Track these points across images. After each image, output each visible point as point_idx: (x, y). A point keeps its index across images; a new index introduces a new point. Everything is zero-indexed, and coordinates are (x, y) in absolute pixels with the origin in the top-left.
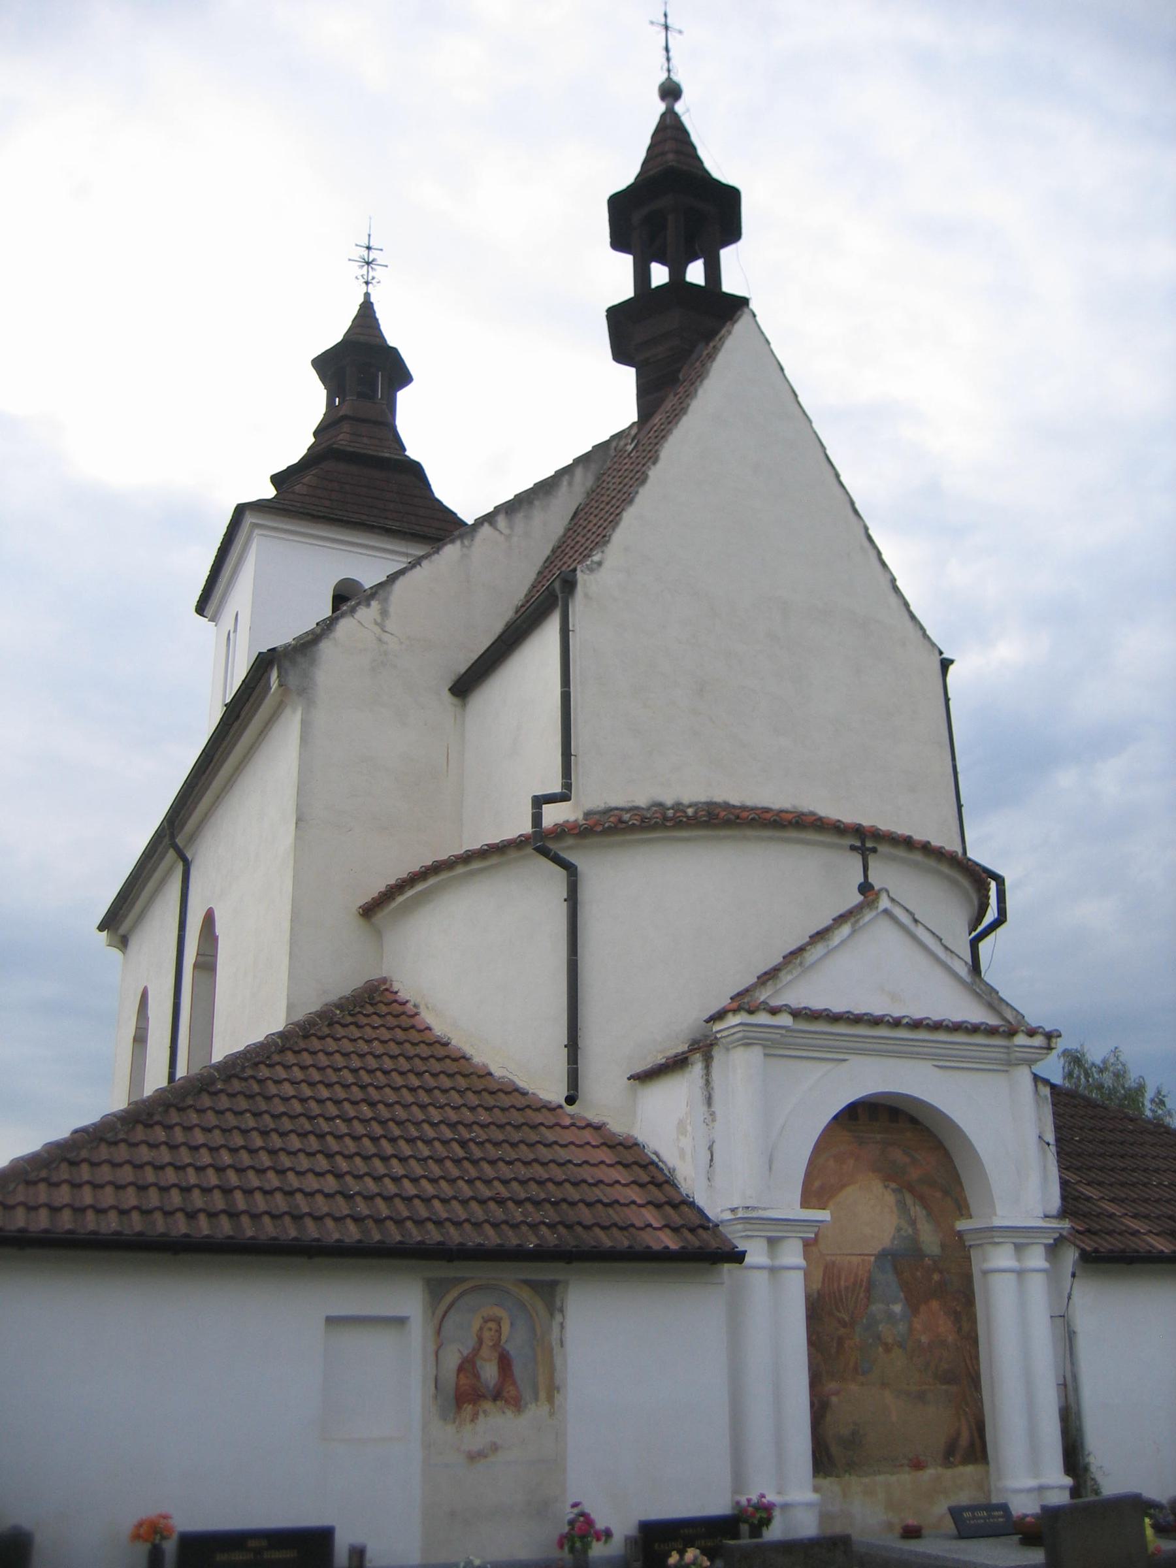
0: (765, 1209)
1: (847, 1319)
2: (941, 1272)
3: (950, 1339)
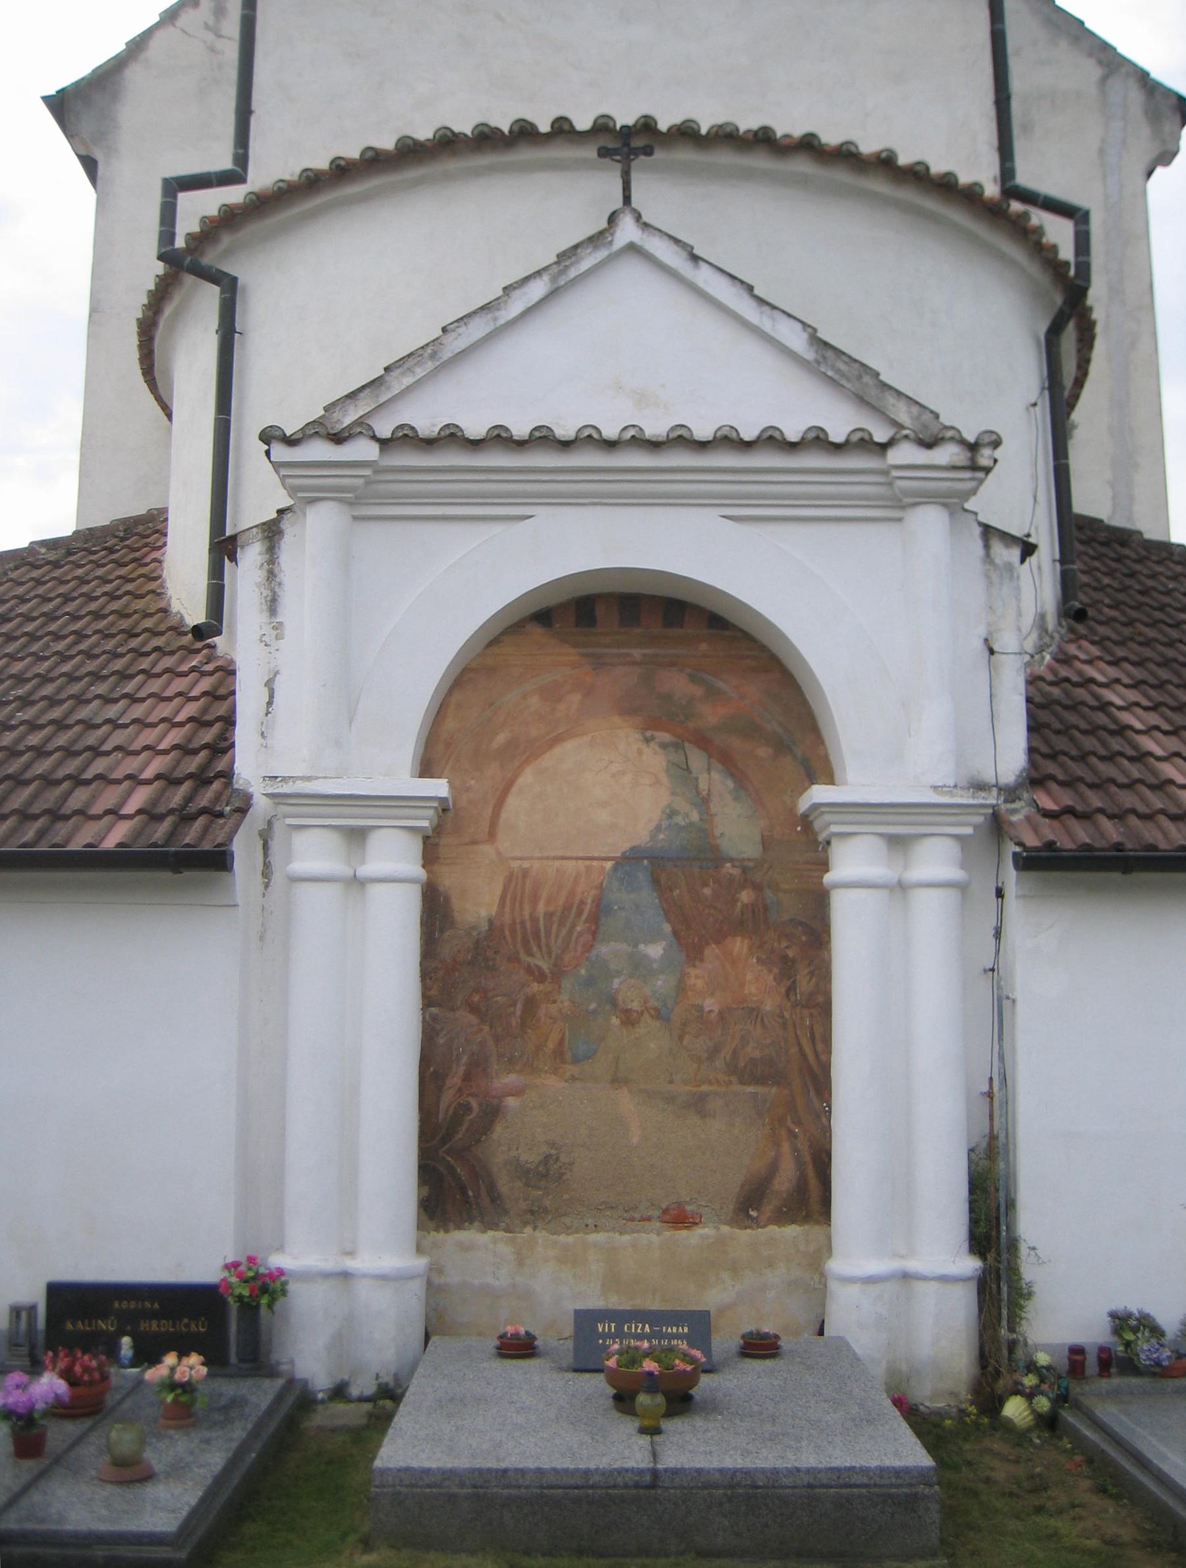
0: (309, 779)
2: (758, 888)
3: (768, 1006)
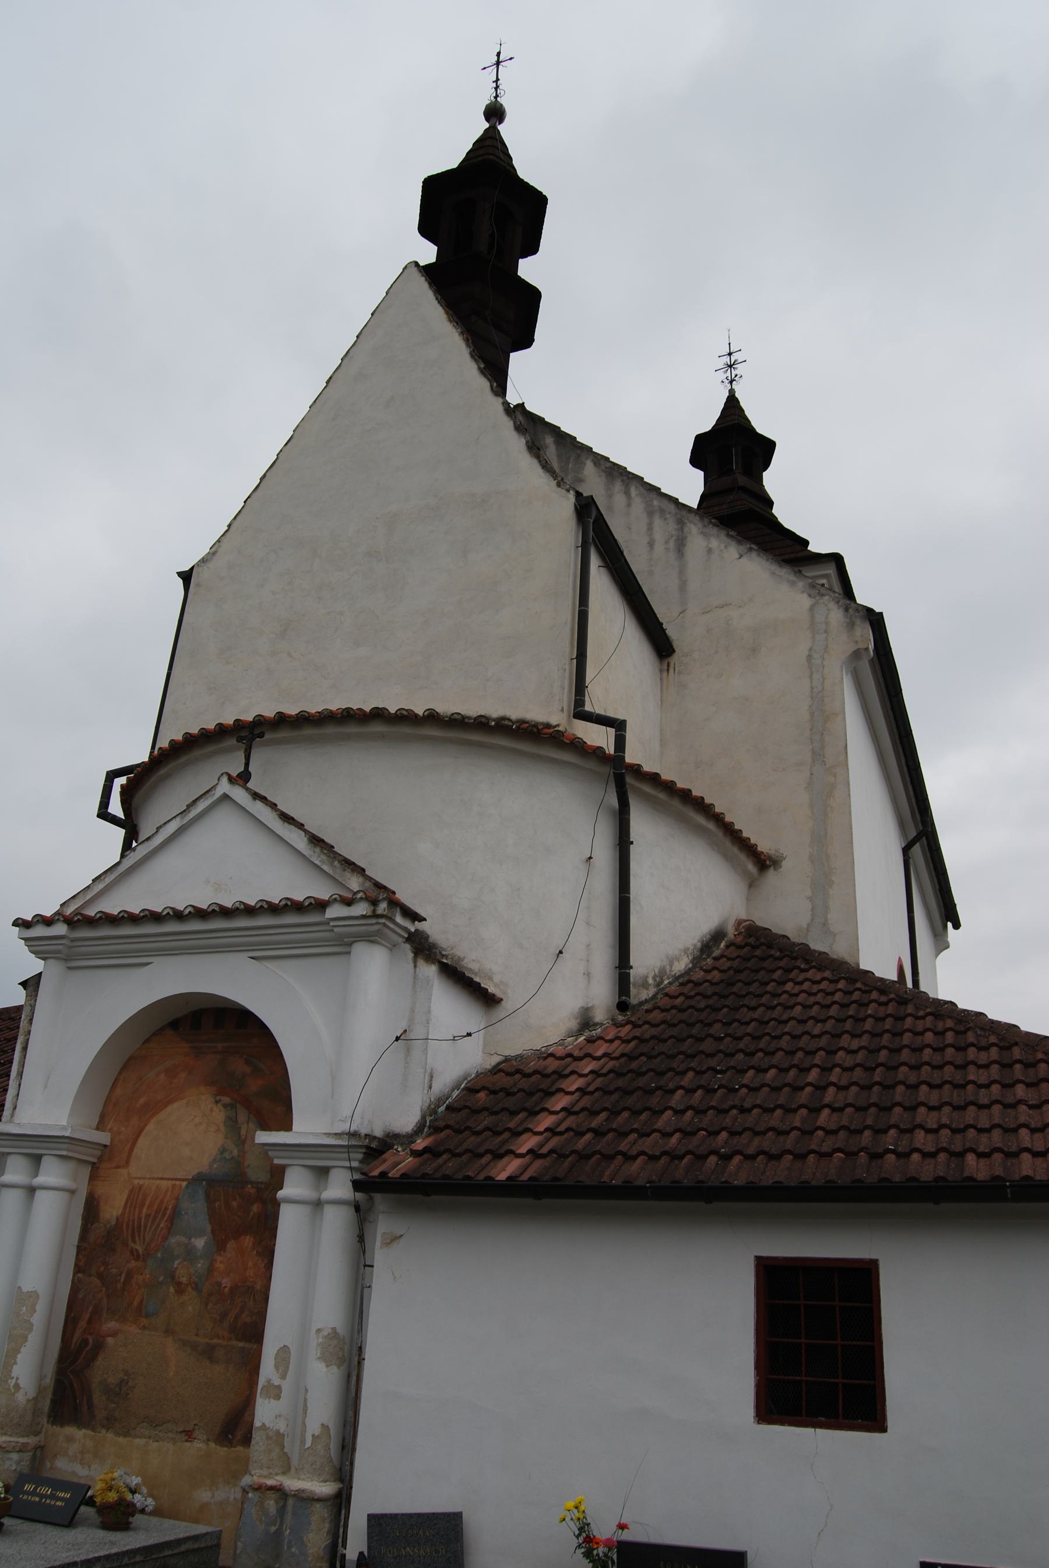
1: (140, 1250)
